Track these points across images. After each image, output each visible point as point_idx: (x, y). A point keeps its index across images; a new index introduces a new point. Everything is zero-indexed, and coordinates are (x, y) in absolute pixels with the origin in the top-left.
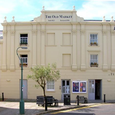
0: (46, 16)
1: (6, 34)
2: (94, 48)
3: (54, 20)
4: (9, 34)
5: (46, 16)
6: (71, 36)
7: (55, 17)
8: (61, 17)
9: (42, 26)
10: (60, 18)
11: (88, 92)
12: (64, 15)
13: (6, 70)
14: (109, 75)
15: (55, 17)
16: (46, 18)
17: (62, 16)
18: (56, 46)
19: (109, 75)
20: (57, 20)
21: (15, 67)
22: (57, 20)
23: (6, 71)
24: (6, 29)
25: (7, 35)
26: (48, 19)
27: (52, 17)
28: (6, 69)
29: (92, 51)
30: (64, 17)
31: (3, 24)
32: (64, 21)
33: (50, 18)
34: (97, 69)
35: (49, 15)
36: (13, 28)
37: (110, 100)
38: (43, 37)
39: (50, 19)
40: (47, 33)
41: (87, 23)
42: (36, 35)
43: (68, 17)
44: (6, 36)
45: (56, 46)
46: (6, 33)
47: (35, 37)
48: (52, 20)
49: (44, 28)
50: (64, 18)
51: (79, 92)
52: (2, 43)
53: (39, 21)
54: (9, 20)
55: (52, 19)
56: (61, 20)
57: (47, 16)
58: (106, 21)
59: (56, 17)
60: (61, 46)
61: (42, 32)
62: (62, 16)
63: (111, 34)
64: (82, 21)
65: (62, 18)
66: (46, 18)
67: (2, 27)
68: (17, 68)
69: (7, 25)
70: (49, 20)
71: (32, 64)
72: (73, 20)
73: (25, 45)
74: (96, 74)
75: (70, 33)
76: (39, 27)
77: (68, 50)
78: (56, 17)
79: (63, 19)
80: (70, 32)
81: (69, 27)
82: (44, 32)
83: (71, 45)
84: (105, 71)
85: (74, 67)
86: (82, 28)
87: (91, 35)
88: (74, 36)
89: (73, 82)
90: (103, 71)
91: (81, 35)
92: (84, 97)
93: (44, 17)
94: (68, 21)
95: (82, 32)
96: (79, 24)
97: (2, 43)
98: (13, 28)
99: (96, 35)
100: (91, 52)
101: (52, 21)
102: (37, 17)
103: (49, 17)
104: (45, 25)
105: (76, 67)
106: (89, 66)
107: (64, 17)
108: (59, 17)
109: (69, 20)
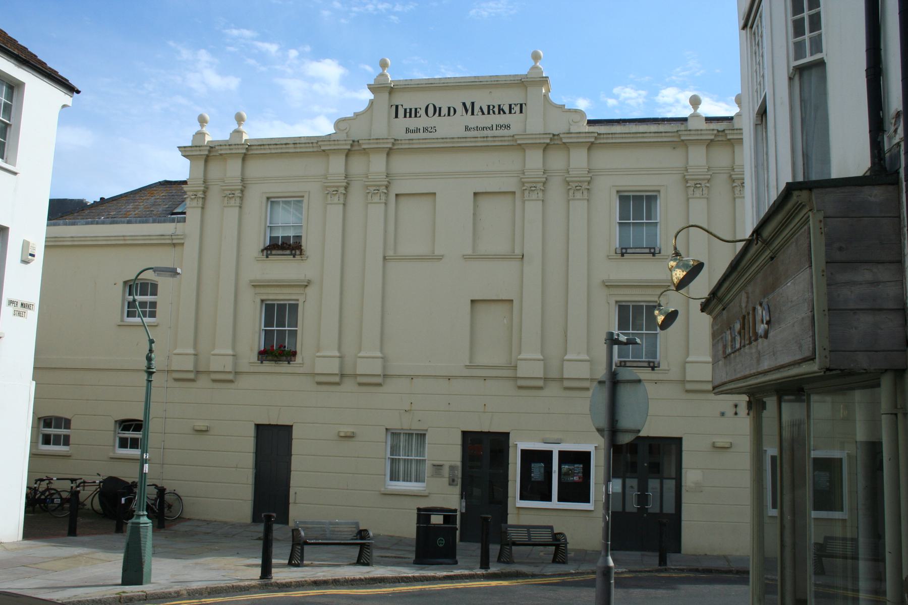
0: (397, 107)
1: (200, 201)
2: (283, 268)
3: (434, 129)
4: (356, 196)
5: (397, 107)
6: (518, 203)
7: (437, 111)
8: (467, 111)
9: (691, 149)
10: (462, 120)
11: (224, 483)
12: (482, 99)
13: (337, 379)
14: (723, 414)
15: (437, 111)
16: (397, 116)
17: (473, 104)
18: (440, 258)
19: (723, 414)
20: (450, 127)
21: (235, 364)
22: (450, 127)
23: (337, 384)
24: (201, 175)
25: (345, 201)
26: (403, 122)
27: (422, 112)
28: (337, 372)
29: (268, 286)
30: (486, 111)
31: (186, 151)
32: (483, 129)
33: (413, 119)
34: (485, 379)
35: (407, 101)
36: (233, 169)
37: (725, 558)
38: (376, 211)
39: (412, 123)
40: (397, 195)
41: (609, 132)
42: (383, 205)
43: (507, 109)
44: (203, 208)
45: (440, 258)
46: (200, 195)
47: (232, 214)
48: (425, 130)
49: (540, 165)
50: (486, 116)
51: (555, 503)
52: (183, 244)
53: (358, 132)
54: (215, 134)
55: (422, 121)
56: (467, 128)
57: (400, 107)
58: (591, 122)
59: (444, 111)
60: (466, 258)
61: (691, 183)
62: (473, 104)
63: (734, 192)
64: (574, 129)
65: (473, 114)
66: (397, 116)
67: (187, 162)
68: (244, 366)
69: (207, 156)
70: (408, 130)
71: (688, 355)
72: (533, 124)
73: (288, 252)
74: (274, 395)
75: (514, 193)
76: (557, 161)
77: (496, 280)
78: (444, 111)
79: (479, 120)
80: (510, 184)
81: (508, 162)
82: (384, 189)
83: (518, 251)
84: (690, 389)
85: (530, 369)
86: (691, 163)
87: (624, 199)
88: (533, 209)
89: (814, 454)
90: (688, 391)
91: (734, 199)
92: (551, 528)
93: (383, 112)
94: (505, 132)
95: (580, 187)
96: (553, 143)
97: (183, 244)
98: (233, 169)
99: (651, 199)
100: (262, 290)
101: (422, 135)
102: (350, 114)
103: (411, 113)
104: (708, 146)
105: (537, 371)
106: (254, 357)
107: (486, 111)
108: (460, 109)
109: (508, 127)
